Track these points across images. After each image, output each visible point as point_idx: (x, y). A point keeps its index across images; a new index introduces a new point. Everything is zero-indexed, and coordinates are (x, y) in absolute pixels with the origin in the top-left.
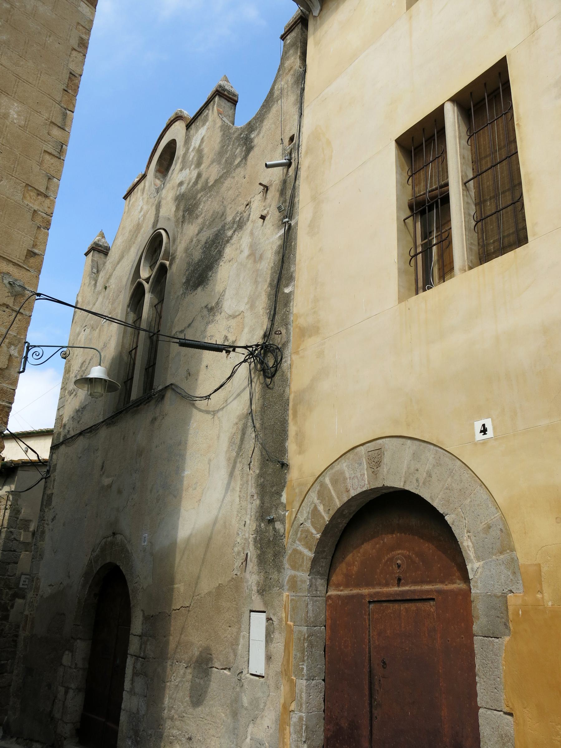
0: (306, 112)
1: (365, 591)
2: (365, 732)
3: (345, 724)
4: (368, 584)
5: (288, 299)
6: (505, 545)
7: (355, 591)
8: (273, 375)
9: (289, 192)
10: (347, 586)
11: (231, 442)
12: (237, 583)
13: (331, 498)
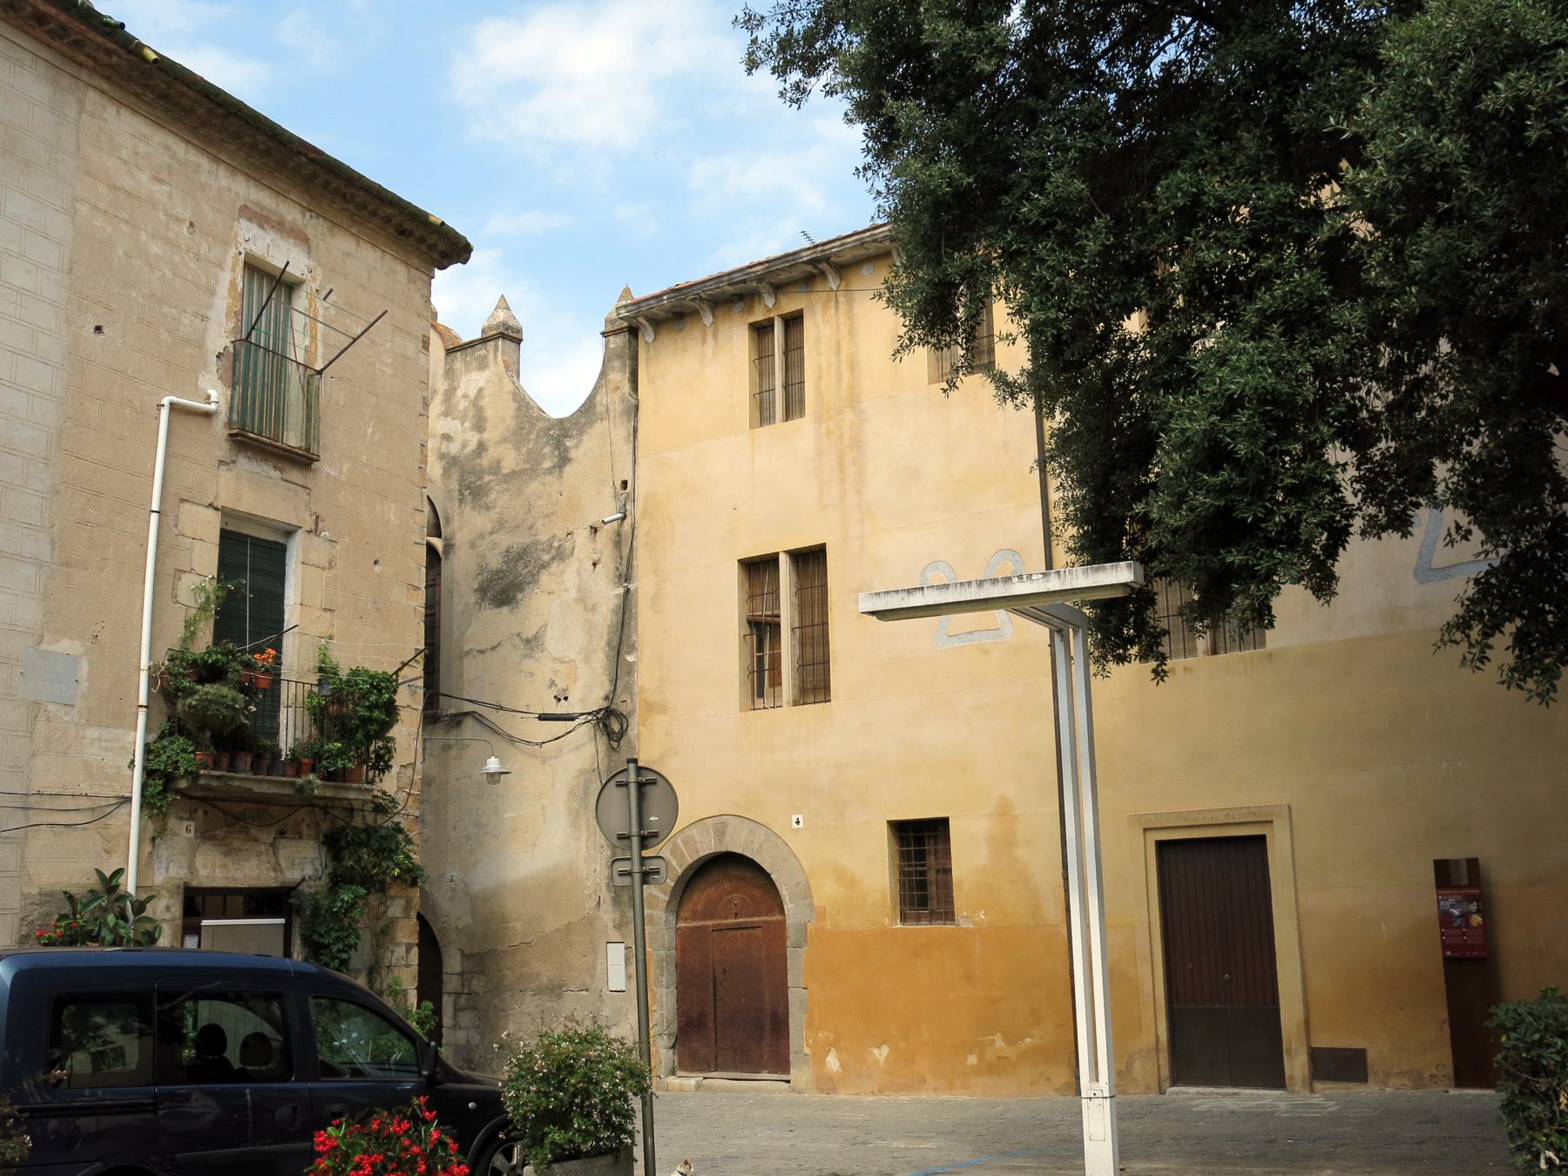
0: (640, 461)
1: (709, 923)
2: (711, 1017)
3: (694, 1015)
4: (711, 918)
5: (630, 669)
6: (807, 895)
7: (701, 923)
8: (619, 741)
9: (625, 551)
10: (693, 919)
11: (572, 793)
12: (590, 922)
13: (683, 856)
